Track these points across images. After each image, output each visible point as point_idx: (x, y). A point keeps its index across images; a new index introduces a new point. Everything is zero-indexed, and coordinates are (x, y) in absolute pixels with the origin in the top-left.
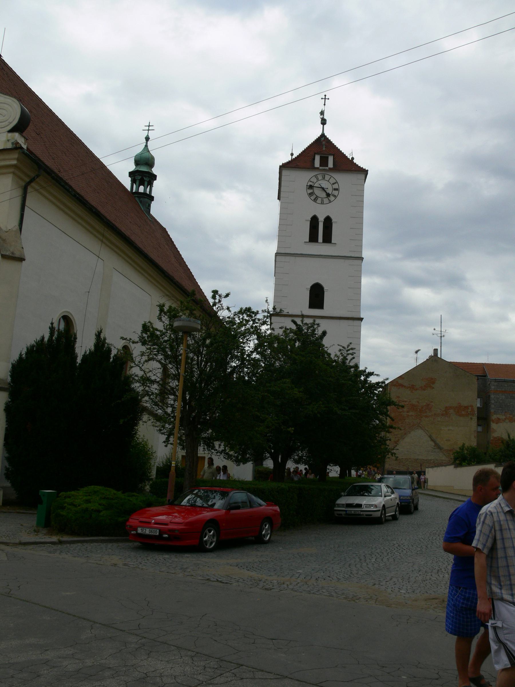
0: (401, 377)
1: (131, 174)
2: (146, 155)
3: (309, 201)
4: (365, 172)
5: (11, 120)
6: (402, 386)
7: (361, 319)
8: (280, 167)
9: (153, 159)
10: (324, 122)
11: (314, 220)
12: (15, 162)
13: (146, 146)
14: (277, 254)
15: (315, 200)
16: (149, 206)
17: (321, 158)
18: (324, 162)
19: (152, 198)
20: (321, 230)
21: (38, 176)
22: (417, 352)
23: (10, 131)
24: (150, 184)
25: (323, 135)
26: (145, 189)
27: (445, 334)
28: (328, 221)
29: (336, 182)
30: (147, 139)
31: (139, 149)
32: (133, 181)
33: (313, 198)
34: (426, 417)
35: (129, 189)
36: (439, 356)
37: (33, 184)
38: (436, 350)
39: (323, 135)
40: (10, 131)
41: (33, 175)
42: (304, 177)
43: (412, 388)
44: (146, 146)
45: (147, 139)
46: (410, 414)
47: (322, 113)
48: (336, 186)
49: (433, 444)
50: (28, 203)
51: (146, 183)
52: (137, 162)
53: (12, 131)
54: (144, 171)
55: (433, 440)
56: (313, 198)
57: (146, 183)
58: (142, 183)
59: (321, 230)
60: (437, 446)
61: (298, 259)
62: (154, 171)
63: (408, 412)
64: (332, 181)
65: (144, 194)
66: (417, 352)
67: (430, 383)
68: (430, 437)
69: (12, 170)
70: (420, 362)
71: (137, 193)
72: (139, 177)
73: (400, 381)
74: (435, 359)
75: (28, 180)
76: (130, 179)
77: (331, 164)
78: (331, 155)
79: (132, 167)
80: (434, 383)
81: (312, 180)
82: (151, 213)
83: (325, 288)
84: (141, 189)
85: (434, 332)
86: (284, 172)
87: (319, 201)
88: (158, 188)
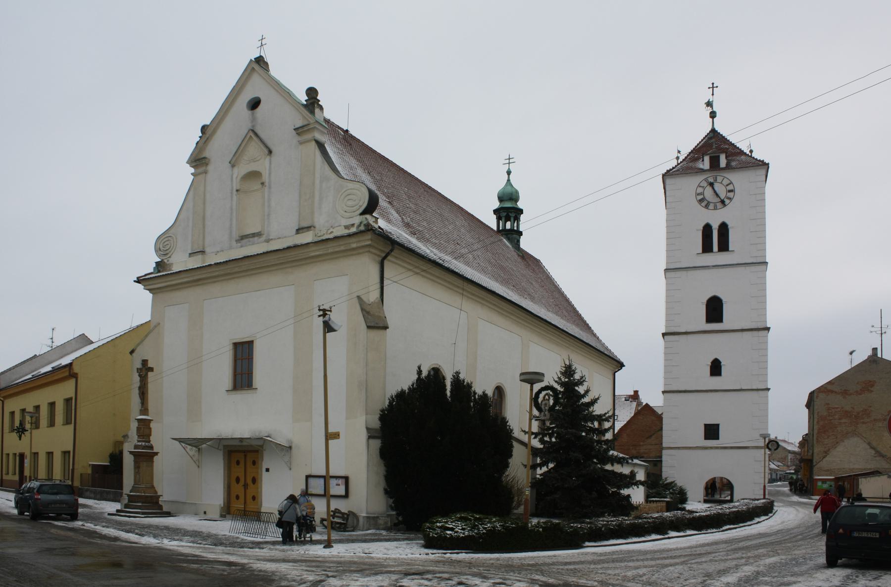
0: (830, 383)
1: (495, 212)
2: (509, 189)
3: (701, 209)
4: (764, 165)
5: (361, 203)
6: (832, 392)
7: (768, 329)
8: (664, 175)
9: (517, 192)
10: (713, 115)
11: (707, 230)
12: (369, 243)
13: (509, 180)
14: (666, 270)
15: (707, 207)
16: (518, 241)
17: (711, 159)
18: (715, 164)
19: (521, 234)
20: (715, 239)
21: (392, 251)
22: (851, 353)
23: (362, 214)
24: (517, 219)
25: (713, 131)
26: (512, 225)
27: (887, 330)
28: (724, 228)
29: (731, 183)
30: (509, 173)
31: (501, 184)
32: (499, 219)
33: (704, 204)
34: (863, 423)
35: (495, 228)
36: (879, 355)
37: (389, 258)
38: (875, 350)
39: (713, 131)
40: (362, 214)
41: (387, 251)
42: (691, 184)
43: (845, 393)
44: (509, 180)
45: (509, 173)
46: (843, 421)
47: (709, 104)
48: (730, 187)
49: (873, 452)
50: (386, 274)
51: (512, 219)
52: (501, 199)
53: (363, 213)
54: (509, 209)
55: (872, 448)
56: (704, 204)
57: (512, 219)
58: (508, 219)
59: (715, 239)
60: (880, 454)
61: (691, 273)
62: (520, 205)
63: (840, 419)
64: (726, 182)
65: (511, 230)
66: (851, 353)
67: (868, 386)
68: (869, 444)
69: (367, 249)
70: (855, 363)
71: (505, 230)
72: (504, 214)
73: (830, 387)
74: (874, 359)
75: (384, 255)
76: (495, 216)
77: (723, 162)
78: (722, 152)
79: (496, 205)
80: (872, 386)
81: (702, 184)
82: (522, 246)
83: (724, 300)
84: (508, 225)
85: (873, 329)
86: (668, 181)
87: (711, 206)
88: (525, 223)
